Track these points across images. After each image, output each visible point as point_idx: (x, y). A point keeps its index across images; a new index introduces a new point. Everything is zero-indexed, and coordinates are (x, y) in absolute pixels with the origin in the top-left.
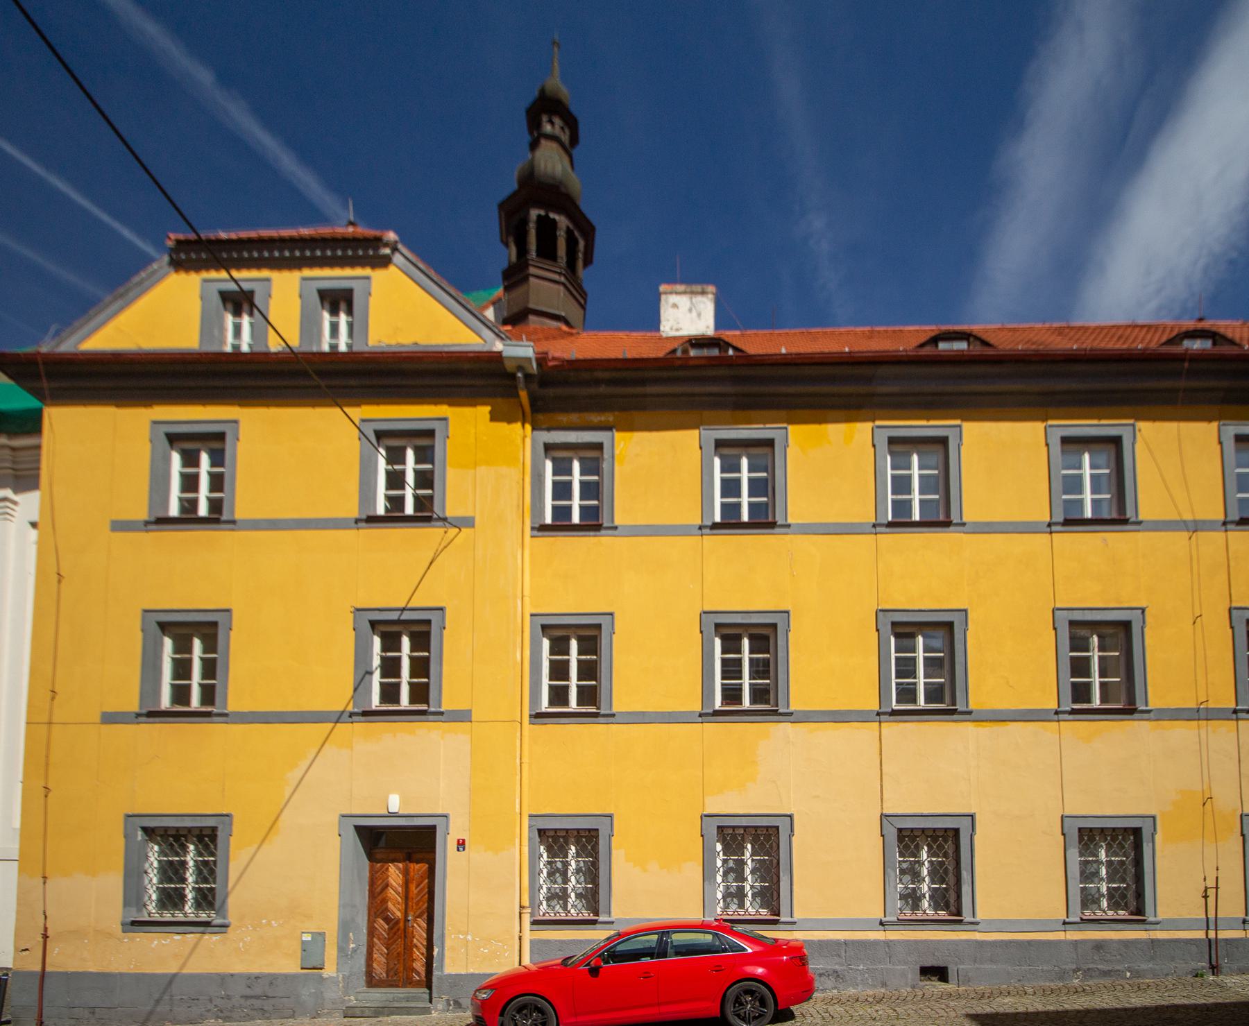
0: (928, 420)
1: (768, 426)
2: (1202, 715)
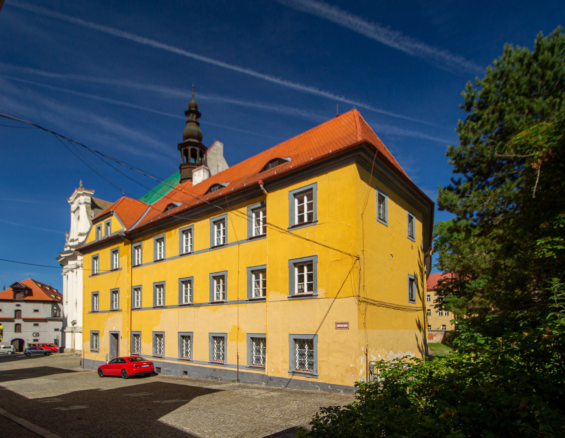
0: (188, 224)
1: (221, 214)
2: (239, 302)
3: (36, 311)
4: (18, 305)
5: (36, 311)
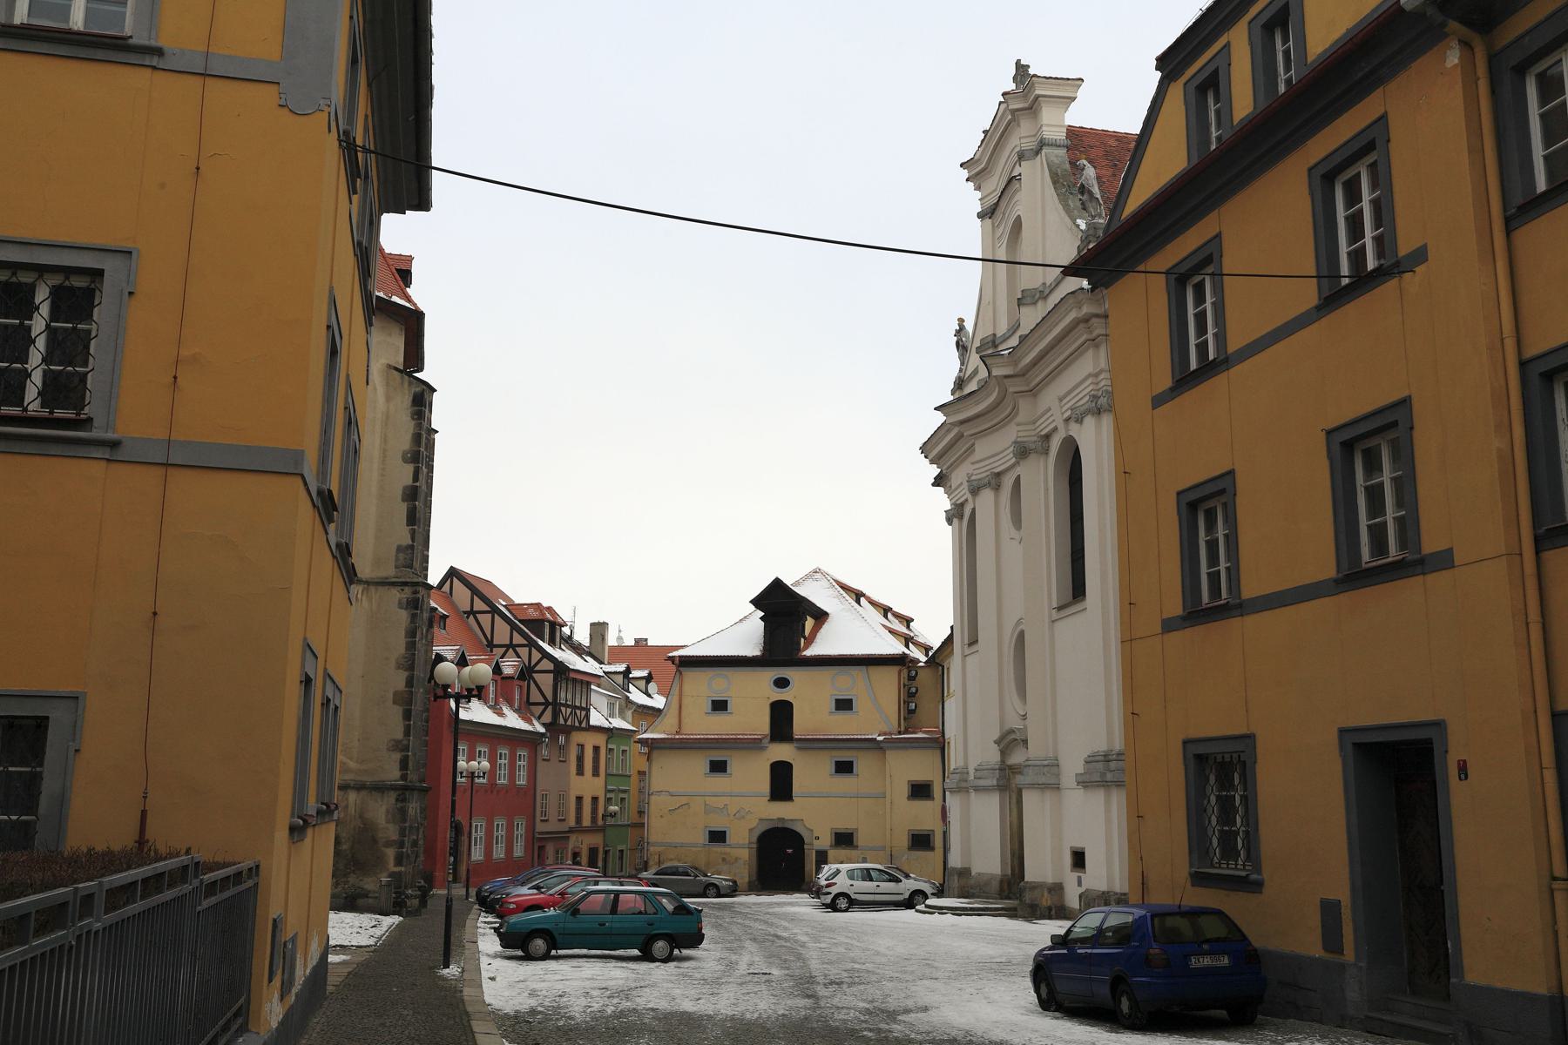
3: (844, 705)
4: (782, 683)
5: (844, 705)
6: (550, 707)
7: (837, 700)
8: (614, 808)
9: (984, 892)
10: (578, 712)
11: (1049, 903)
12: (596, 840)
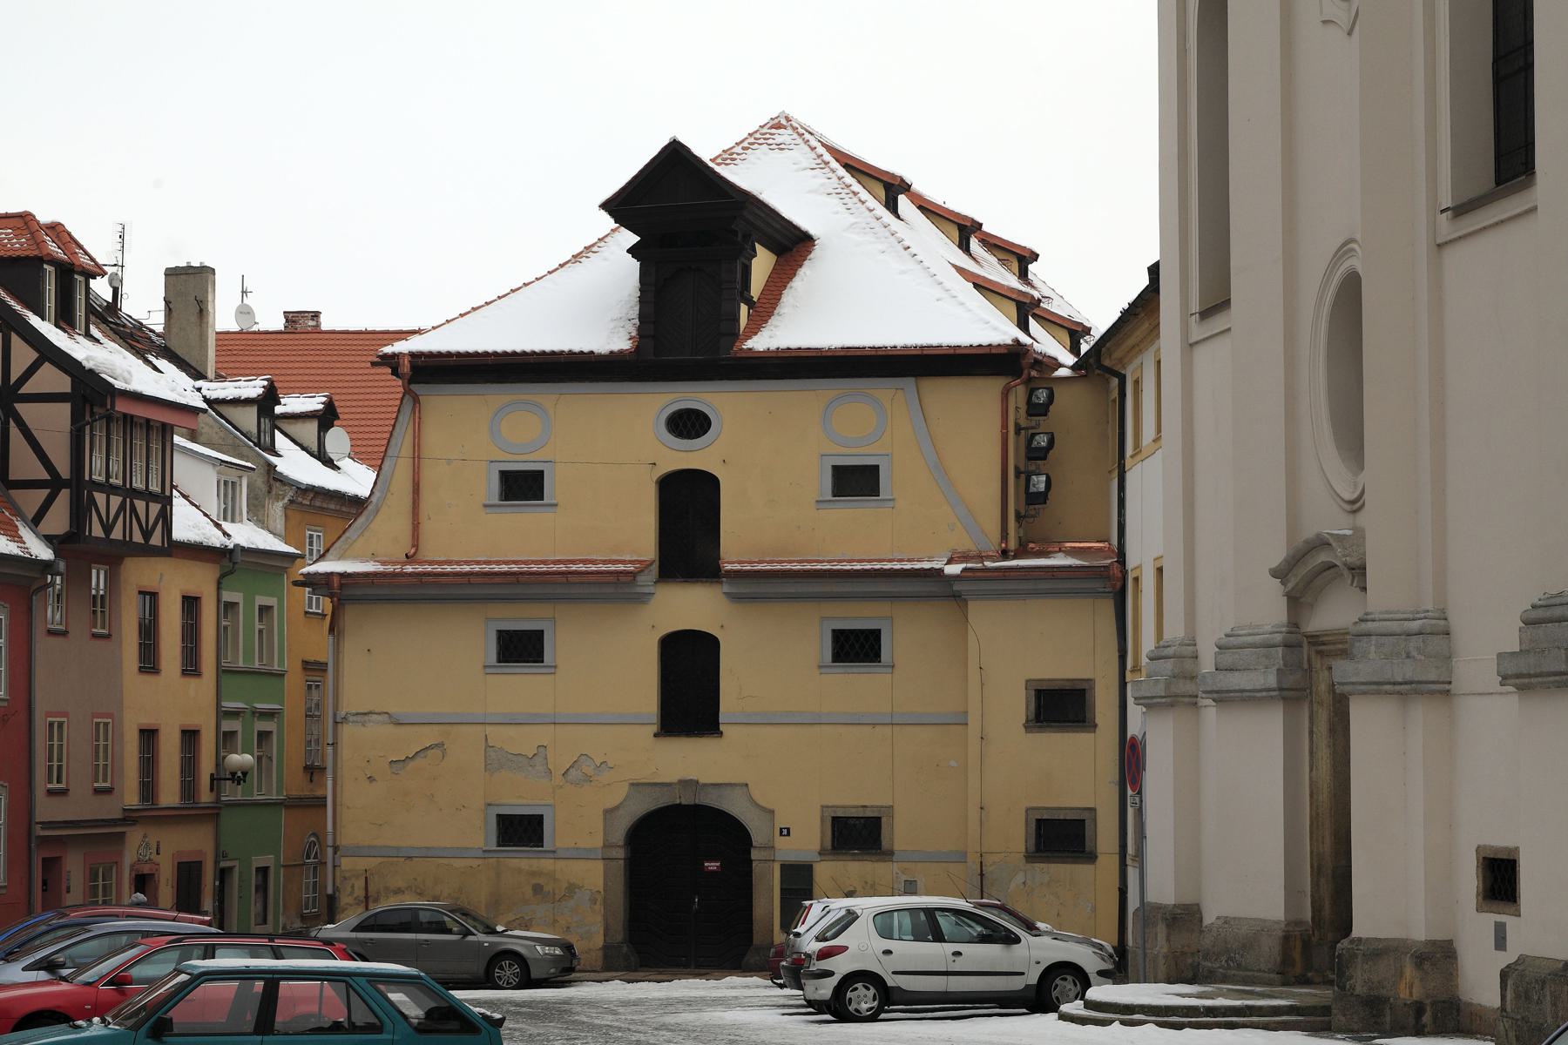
4: (689, 424)
6: (64, 495)
7: (837, 470)
8: (240, 759)
9: (1239, 966)
10: (140, 505)
11: (1417, 994)
12: (195, 841)
